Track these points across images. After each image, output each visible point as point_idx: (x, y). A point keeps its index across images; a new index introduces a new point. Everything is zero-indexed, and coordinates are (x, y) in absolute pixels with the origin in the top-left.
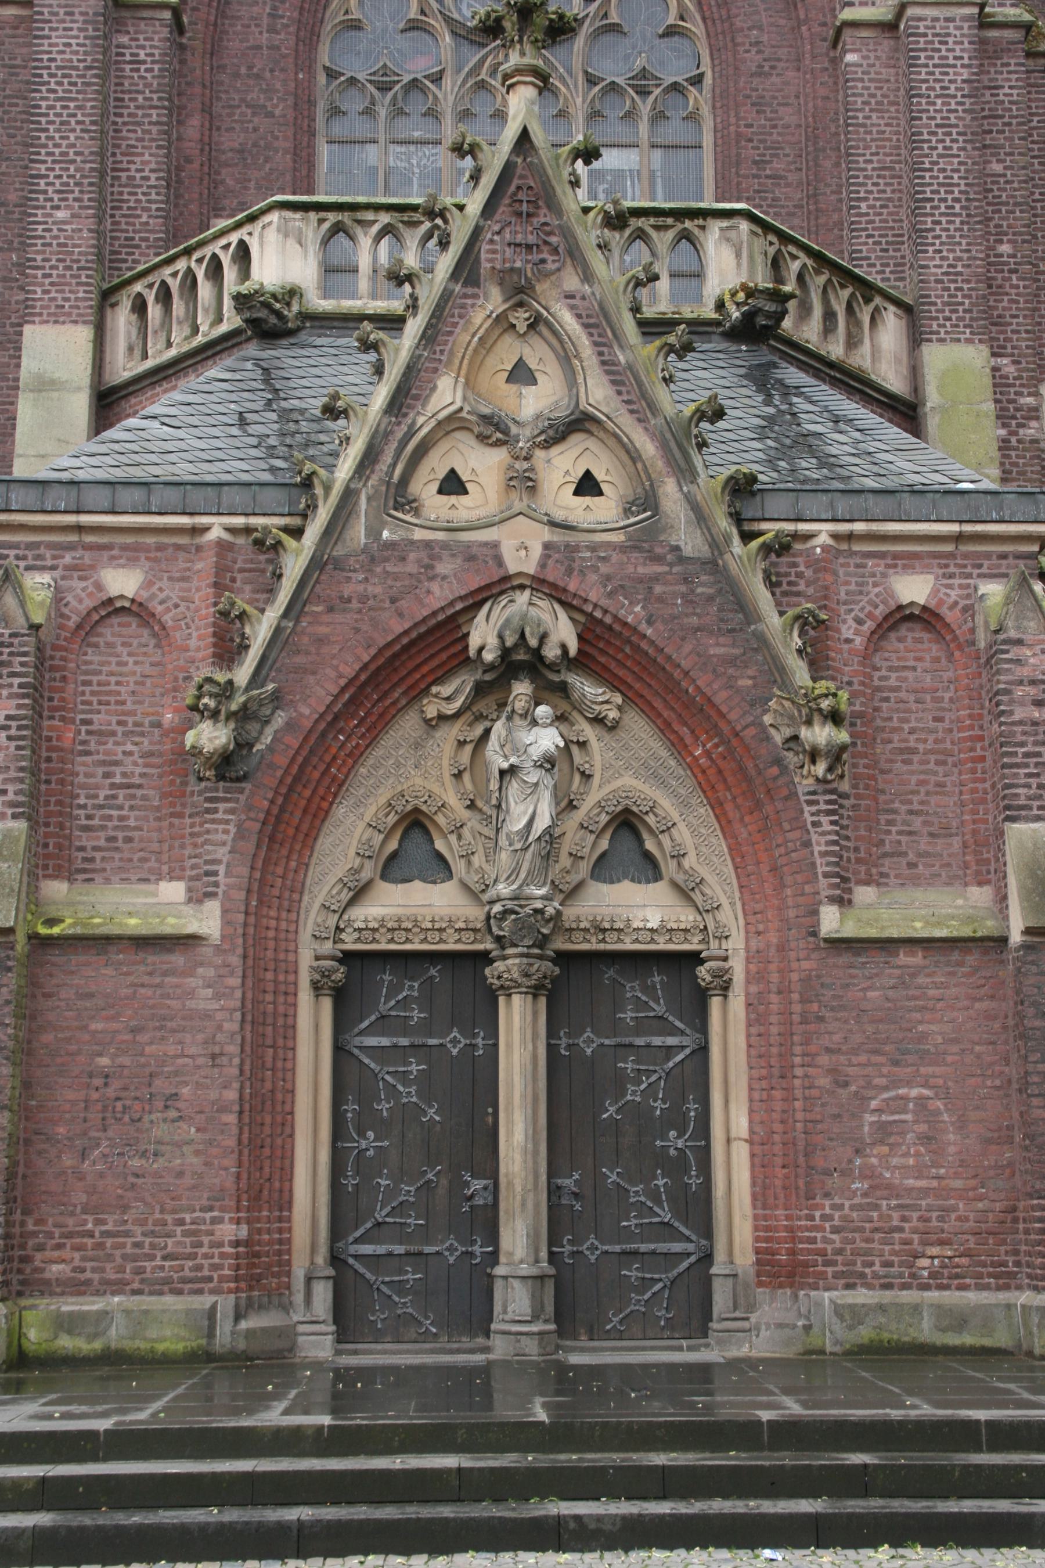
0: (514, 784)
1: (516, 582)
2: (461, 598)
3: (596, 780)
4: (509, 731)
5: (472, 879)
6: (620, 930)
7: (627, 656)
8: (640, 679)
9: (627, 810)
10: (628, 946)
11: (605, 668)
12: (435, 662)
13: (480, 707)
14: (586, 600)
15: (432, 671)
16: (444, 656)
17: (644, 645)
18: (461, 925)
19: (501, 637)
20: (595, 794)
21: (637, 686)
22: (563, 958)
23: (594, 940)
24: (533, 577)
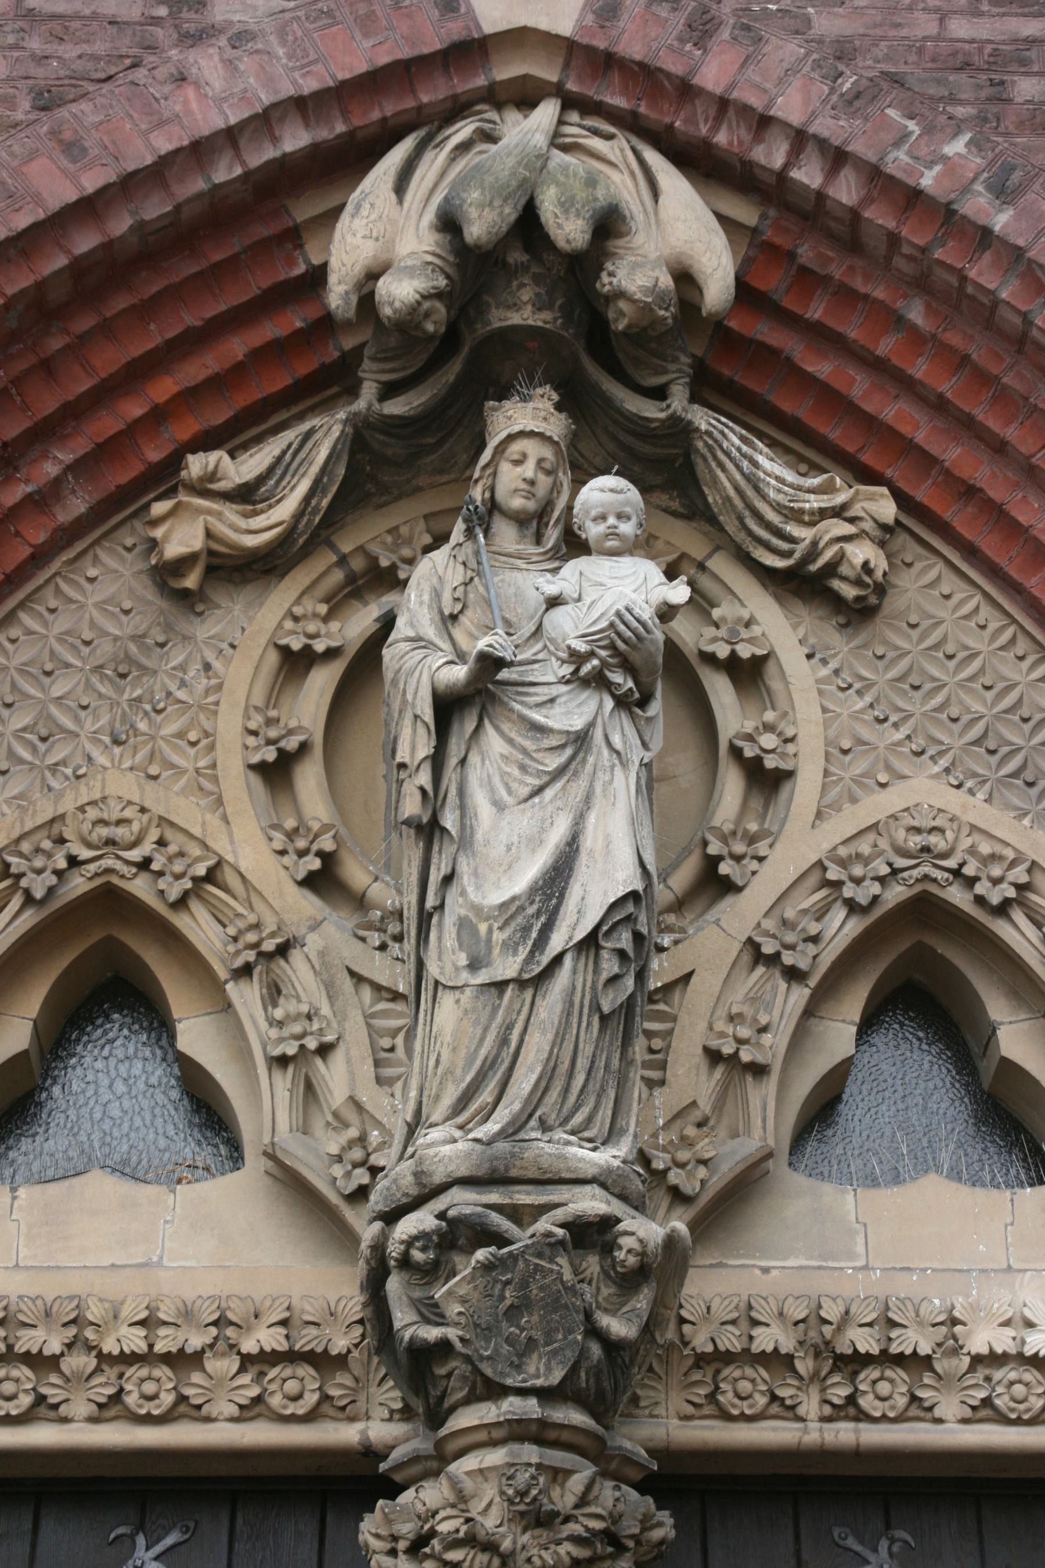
0: (493, 741)
1: (507, 70)
2: (302, 106)
3: (805, 791)
4: (475, 572)
5: (320, 1156)
6: (915, 1363)
7: (917, 339)
8: (968, 426)
9: (924, 910)
10: (952, 1431)
11: (833, 399)
12: (195, 370)
13: (366, 535)
14: (764, 123)
16: (237, 347)
17: (982, 273)
18: (266, 1338)
19: (449, 224)
20: (800, 839)
21: (952, 453)
22: (682, 1481)
23: (810, 1406)
24: (570, 49)
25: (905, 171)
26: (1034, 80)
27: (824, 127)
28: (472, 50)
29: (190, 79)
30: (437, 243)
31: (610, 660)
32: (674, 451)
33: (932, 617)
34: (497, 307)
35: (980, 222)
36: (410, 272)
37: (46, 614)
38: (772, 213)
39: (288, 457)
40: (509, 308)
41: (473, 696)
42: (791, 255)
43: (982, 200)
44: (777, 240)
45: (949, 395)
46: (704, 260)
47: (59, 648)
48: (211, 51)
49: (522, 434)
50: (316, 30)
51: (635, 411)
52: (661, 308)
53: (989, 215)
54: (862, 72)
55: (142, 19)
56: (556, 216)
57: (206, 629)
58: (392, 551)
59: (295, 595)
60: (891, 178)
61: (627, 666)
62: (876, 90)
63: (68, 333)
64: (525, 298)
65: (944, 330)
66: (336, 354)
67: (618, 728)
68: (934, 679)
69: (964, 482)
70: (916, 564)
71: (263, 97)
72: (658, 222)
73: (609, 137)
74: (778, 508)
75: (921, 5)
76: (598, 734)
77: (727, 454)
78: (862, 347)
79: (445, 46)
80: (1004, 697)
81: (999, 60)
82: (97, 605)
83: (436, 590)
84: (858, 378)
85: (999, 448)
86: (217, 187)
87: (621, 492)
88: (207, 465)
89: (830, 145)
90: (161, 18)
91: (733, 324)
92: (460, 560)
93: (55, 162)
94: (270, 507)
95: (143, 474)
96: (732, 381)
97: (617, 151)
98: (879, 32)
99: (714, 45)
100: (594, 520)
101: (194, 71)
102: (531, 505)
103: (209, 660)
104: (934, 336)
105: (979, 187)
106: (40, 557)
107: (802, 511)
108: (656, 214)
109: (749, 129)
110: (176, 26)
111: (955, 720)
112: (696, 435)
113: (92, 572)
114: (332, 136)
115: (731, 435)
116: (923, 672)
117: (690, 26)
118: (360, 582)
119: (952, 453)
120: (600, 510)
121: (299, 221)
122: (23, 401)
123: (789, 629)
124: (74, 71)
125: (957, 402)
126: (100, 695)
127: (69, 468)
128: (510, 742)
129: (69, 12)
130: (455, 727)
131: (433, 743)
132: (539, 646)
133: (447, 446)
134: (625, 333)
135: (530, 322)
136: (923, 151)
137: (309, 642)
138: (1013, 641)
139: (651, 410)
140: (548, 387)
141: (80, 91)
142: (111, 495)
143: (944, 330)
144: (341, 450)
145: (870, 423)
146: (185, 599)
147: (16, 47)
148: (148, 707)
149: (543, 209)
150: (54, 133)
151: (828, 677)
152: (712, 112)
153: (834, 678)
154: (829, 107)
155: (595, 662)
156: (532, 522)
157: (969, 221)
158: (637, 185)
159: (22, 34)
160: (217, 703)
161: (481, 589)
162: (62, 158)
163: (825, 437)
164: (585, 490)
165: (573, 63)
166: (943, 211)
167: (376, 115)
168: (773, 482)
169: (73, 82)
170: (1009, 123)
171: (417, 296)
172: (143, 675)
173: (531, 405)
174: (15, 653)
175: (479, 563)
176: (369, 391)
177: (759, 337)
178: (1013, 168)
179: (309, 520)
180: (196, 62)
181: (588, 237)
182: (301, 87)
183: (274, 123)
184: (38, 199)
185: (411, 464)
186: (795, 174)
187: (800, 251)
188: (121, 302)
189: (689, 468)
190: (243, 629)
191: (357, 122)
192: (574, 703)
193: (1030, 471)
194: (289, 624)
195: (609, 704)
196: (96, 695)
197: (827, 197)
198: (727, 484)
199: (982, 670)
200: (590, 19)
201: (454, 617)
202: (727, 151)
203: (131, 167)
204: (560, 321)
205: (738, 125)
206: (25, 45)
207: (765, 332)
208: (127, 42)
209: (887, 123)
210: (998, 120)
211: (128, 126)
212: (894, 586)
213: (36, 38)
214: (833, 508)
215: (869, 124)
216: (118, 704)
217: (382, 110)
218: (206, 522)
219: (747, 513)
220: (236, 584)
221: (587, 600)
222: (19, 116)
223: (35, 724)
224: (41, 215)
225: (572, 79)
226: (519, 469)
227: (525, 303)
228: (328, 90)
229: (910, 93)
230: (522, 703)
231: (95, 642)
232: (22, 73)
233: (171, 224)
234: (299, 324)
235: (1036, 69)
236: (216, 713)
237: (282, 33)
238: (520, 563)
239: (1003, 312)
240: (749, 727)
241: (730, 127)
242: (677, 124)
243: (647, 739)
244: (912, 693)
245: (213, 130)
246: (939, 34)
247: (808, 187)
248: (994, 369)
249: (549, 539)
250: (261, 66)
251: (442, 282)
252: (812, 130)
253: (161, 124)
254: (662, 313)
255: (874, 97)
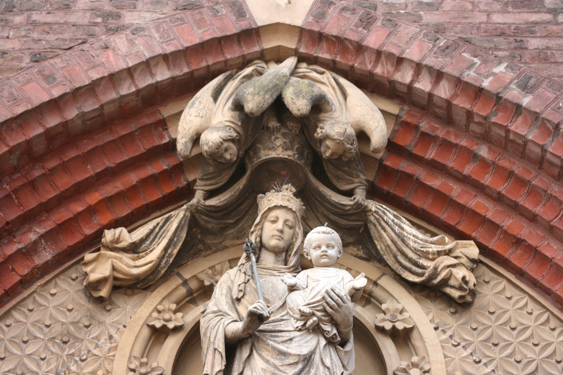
0: (258, 362)
1: (269, 43)
2: (166, 58)
7: (485, 164)
11: (441, 198)
14: (399, 61)
15: (110, 201)
16: (133, 178)
17: (518, 127)
19: (238, 106)
21: (508, 222)
24: (301, 32)
25: (474, 79)
26: (538, 40)
27: (430, 61)
28: (252, 34)
29: (110, 48)
30: (232, 116)
31: (323, 318)
32: (359, 223)
33: (502, 308)
34: (264, 150)
35: (515, 102)
36: (217, 129)
37: (27, 312)
38: (406, 108)
39: (157, 230)
40: (270, 149)
41: (247, 338)
42: (417, 127)
43: (515, 92)
44: (409, 120)
45: (503, 192)
46: (371, 123)
47: (32, 329)
48: (122, 36)
49: (276, 207)
50: (174, 26)
51: (337, 201)
52: (348, 144)
53: (519, 98)
54: (449, 38)
55: (89, 24)
56: (293, 99)
57: (110, 319)
58: (212, 278)
59: (159, 299)
60: (467, 83)
61: (334, 323)
62: (457, 45)
63: (44, 169)
64: (278, 144)
65: (499, 160)
66: (185, 183)
67: (329, 355)
68: (505, 340)
69: (514, 237)
70: (491, 282)
71: (147, 55)
72: (346, 109)
73: (322, 73)
74: (415, 251)
75: (477, 9)
76: (317, 358)
77: (387, 223)
78: (456, 171)
79: (238, 31)
80: (545, 350)
81: (519, 31)
82: (54, 307)
83: (229, 288)
84: (455, 187)
85: (533, 218)
86: (123, 97)
87: (328, 233)
88: (115, 235)
89: (434, 69)
90: (99, 23)
91: (388, 163)
92: (243, 271)
93: (39, 84)
94: (147, 254)
95: (82, 241)
96: (388, 193)
97: (326, 79)
98: (457, 21)
99: (373, 28)
100: (315, 248)
101: (113, 44)
102: (282, 244)
103: (112, 334)
104: (494, 163)
105: (513, 86)
106: (25, 282)
107: (428, 253)
108: (346, 105)
109: (392, 66)
110: (105, 26)
111: (519, 362)
112: (370, 214)
113: (53, 291)
114: (181, 74)
115: (388, 214)
116: (500, 337)
117: (361, 20)
118: (195, 295)
119: (508, 222)
120: (317, 243)
121: (165, 116)
122: (19, 202)
123: (424, 315)
124: (53, 45)
125: (508, 195)
126: (52, 353)
127: (42, 236)
128: (267, 362)
129: (53, 22)
130: (238, 356)
131: (224, 363)
132: (285, 312)
133: (240, 225)
134: (329, 160)
135: (281, 156)
136: (483, 71)
137: (166, 323)
138: (548, 320)
139: (346, 201)
140: (290, 185)
141: (56, 54)
142: (65, 251)
143: (499, 160)
144: (184, 224)
145: (462, 209)
146: (100, 301)
147: (26, 36)
148: (77, 359)
149: (286, 97)
150: (40, 72)
151: (447, 339)
152: (373, 58)
153: (450, 340)
154: (433, 53)
155: (315, 318)
156: (283, 253)
157: (509, 101)
158: (336, 93)
159: (29, 31)
160: (114, 356)
161: (253, 285)
162: (43, 82)
163: (438, 218)
164: (309, 236)
165: (303, 40)
166: (495, 98)
167: (204, 64)
168: (412, 237)
169: (52, 50)
170: (527, 58)
171: (221, 140)
172: (76, 342)
173: (281, 193)
174: (8, 332)
175: (253, 273)
176: (199, 195)
177: (401, 169)
178: (530, 78)
179: (167, 260)
180: (114, 40)
181: (309, 108)
182: (165, 50)
183: (152, 67)
184: (29, 100)
185: (219, 230)
186: (417, 85)
187: (421, 125)
188: (72, 154)
189: (367, 231)
190: (131, 317)
191: (194, 67)
192: (303, 341)
193: (551, 230)
194: (155, 314)
195: (323, 342)
196: (50, 352)
197: (434, 95)
198: (387, 238)
199: (532, 336)
200: (311, 19)
201: (239, 300)
202: (381, 76)
203: (78, 85)
204: (296, 156)
205: (387, 64)
206: (30, 35)
207: (405, 166)
208: (81, 33)
209: (464, 60)
210: (521, 57)
211: (78, 68)
212: (480, 293)
213: (36, 33)
214: (445, 251)
215: (453, 60)
216: (61, 356)
217: (207, 62)
218: (112, 262)
219: (398, 253)
220: (129, 296)
221: (310, 288)
222: (24, 65)
223: (15, 368)
224: (30, 107)
225: (302, 47)
226: (275, 225)
227: (278, 147)
228: (179, 51)
229: (474, 46)
230: (274, 341)
231: (52, 326)
232: (27, 47)
233: (99, 116)
234: (165, 167)
235: (538, 35)
236: (113, 361)
237: (157, 29)
238: (275, 273)
239: (531, 147)
240: (404, 364)
241: (383, 65)
242: (356, 65)
243: (345, 363)
244: (493, 348)
245: (120, 69)
246: (487, 21)
247: (424, 91)
248: (527, 177)
249: (291, 262)
250: (147, 42)
251: (235, 134)
252: (424, 63)
253: (94, 67)
254: (349, 146)
255: (456, 49)
